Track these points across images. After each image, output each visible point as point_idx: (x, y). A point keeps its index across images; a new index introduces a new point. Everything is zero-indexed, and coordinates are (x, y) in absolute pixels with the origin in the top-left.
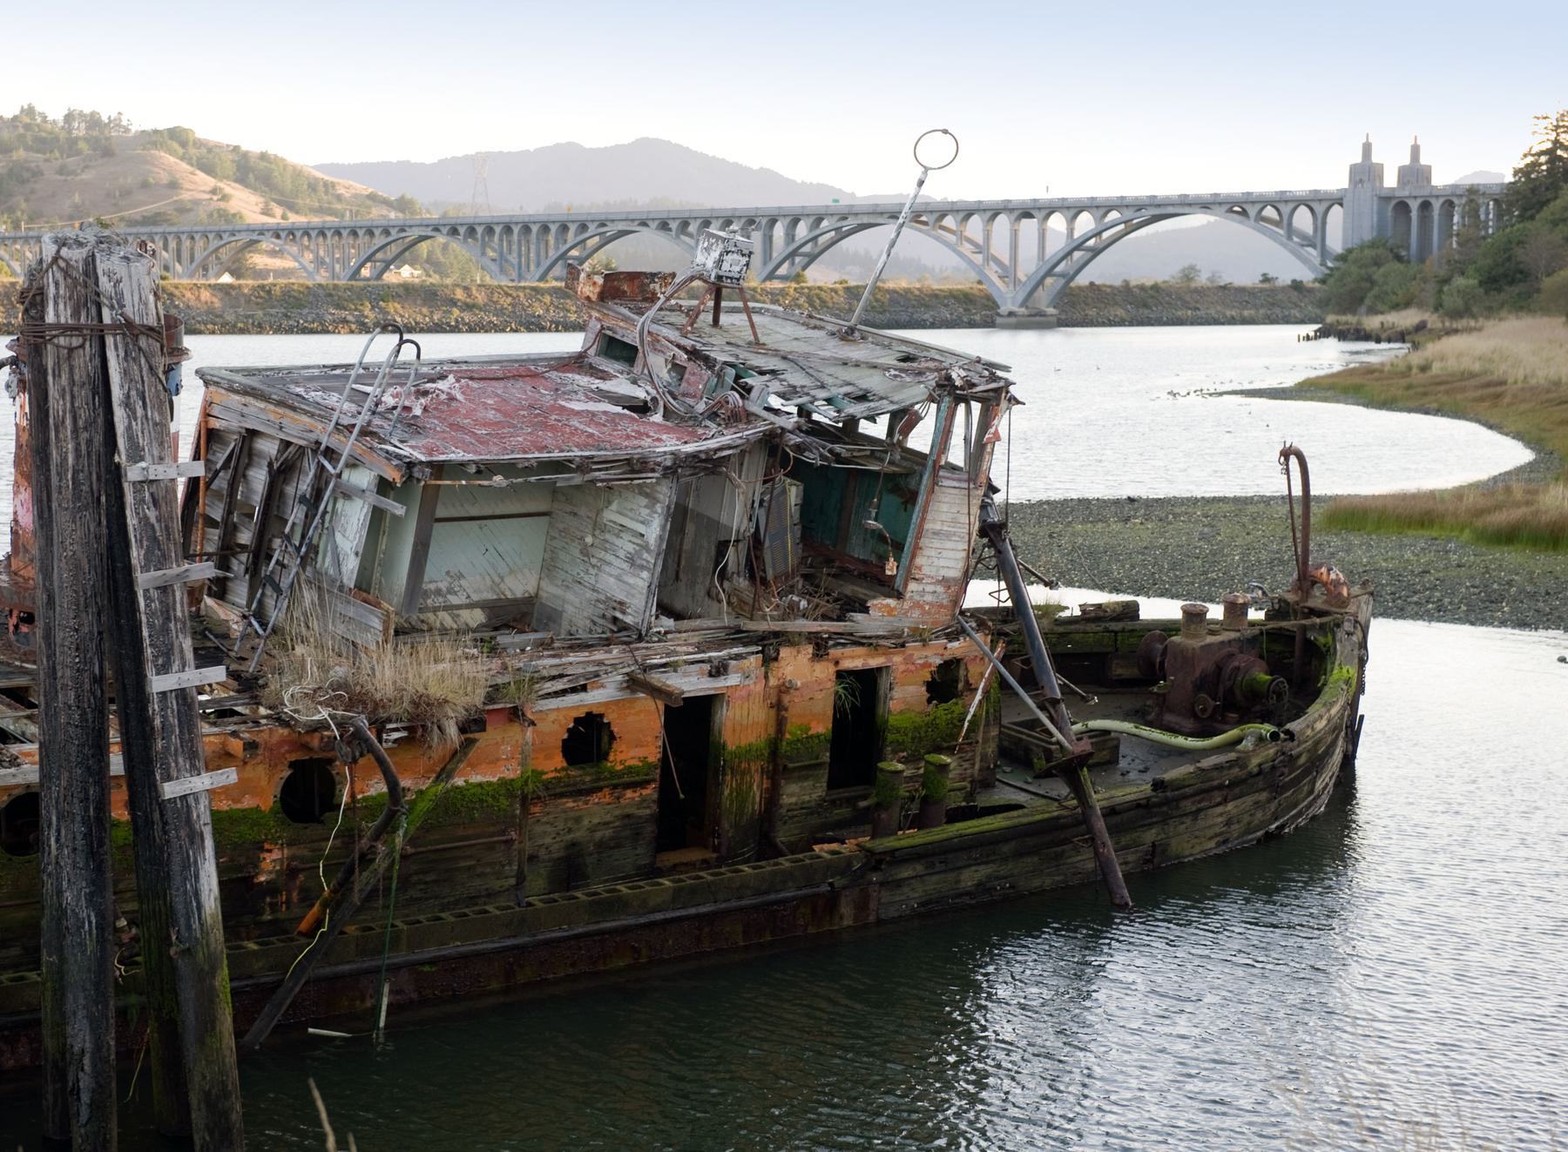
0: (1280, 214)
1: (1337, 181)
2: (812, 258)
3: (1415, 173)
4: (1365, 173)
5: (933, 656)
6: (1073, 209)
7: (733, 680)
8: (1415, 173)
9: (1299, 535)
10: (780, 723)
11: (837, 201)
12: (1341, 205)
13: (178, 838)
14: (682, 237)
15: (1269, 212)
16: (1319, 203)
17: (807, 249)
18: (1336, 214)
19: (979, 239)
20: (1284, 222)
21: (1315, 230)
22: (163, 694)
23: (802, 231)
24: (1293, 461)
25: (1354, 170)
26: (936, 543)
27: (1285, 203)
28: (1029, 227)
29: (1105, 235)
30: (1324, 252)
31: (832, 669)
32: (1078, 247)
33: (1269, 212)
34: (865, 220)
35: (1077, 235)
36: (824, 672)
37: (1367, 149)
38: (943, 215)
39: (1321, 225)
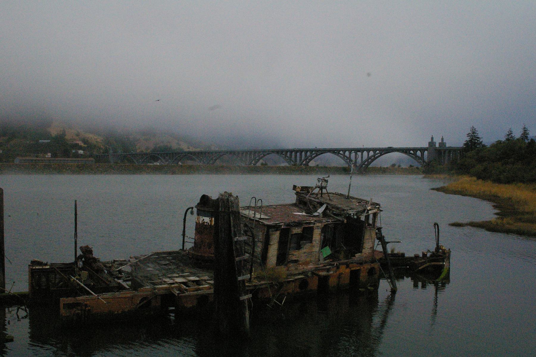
0: (414, 152)
1: (426, 145)
2: (310, 160)
3: (442, 144)
4: (432, 144)
5: (367, 266)
6: (368, 150)
7: (331, 273)
8: (442, 144)
9: (437, 237)
10: (339, 281)
11: (316, 147)
12: (427, 151)
13: (67, 301)
14: (282, 155)
15: (412, 152)
16: (422, 150)
17: (309, 158)
18: (426, 152)
19: (348, 156)
20: (415, 154)
21: (421, 156)
22: (239, 281)
23: (308, 154)
24: (436, 225)
25: (429, 143)
26: (367, 241)
27: (415, 150)
28: (359, 154)
29: (376, 156)
30: (424, 162)
31: (350, 270)
32: (370, 159)
33: (412, 152)
34: (323, 152)
35: (370, 156)
36: (348, 270)
37: (432, 138)
38: (340, 151)
39: (422, 154)
